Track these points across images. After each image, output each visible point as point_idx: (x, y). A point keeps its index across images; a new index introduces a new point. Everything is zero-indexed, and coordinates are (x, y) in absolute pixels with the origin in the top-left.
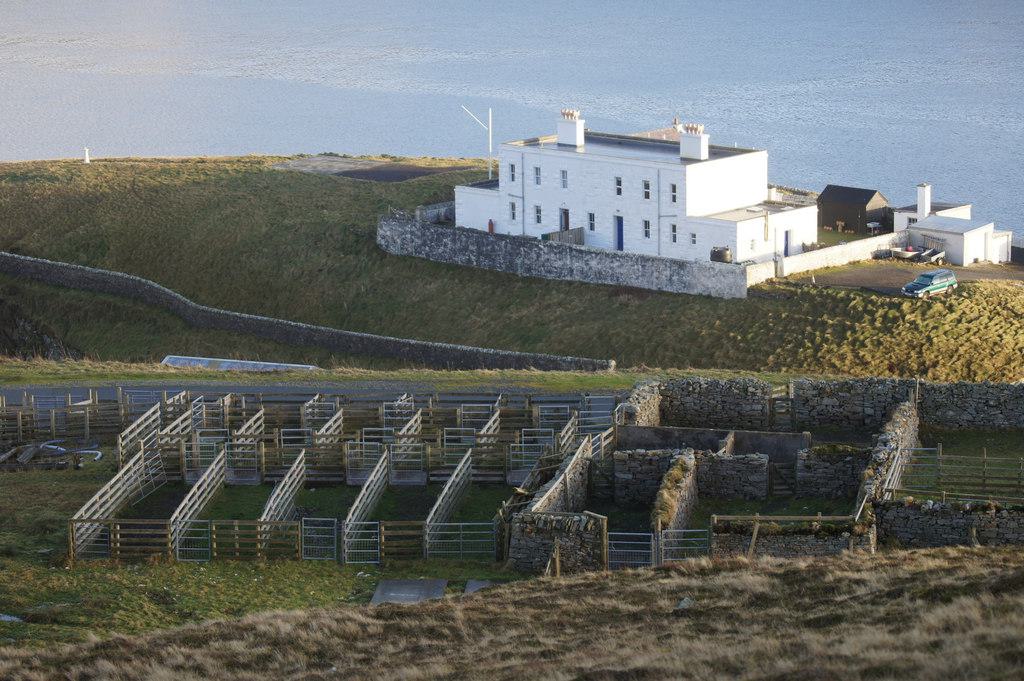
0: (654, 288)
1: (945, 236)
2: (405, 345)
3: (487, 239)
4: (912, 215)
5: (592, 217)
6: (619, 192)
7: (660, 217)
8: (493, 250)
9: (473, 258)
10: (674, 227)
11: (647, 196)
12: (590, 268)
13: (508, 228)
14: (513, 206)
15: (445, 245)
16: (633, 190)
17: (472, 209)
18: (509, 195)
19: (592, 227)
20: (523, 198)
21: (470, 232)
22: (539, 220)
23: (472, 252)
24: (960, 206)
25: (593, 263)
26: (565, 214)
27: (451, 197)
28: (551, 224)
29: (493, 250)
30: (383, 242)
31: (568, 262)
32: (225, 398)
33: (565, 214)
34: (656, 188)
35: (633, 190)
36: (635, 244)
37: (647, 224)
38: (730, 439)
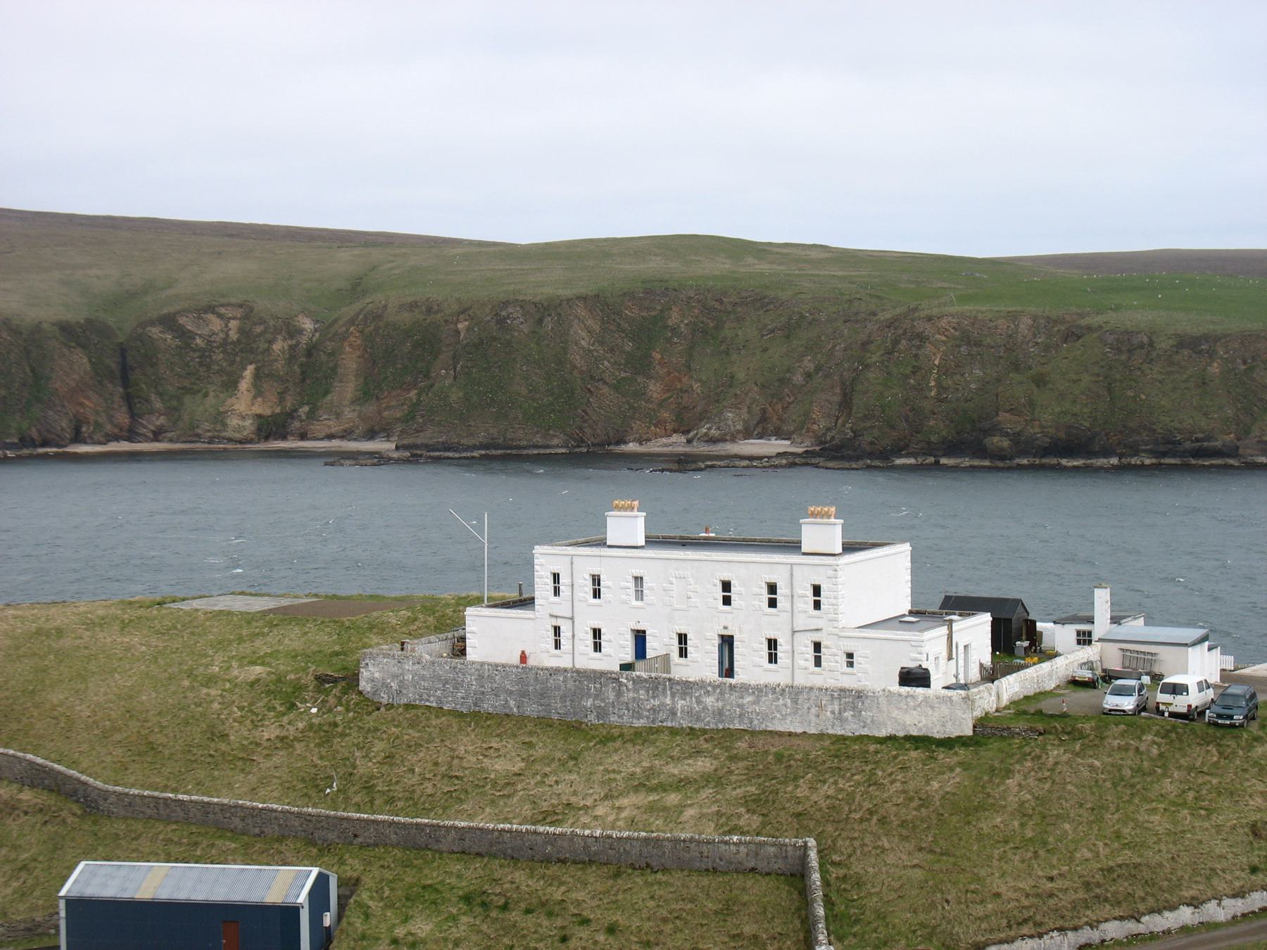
0: (813, 731)
1: (1152, 649)
2: (448, 829)
4: (1084, 627)
5: (682, 638)
6: (727, 601)
7: (794, 632)
10: (817, 647)
11: (772, 603)
12: (705, 708)
13: (545, 657)
14: (557, 630)
16: (749, 594)
18: (552, 616)
19: (683, 653)
20: (572, 618)
22: (597, 647)
25: (709, 701)
27: (460, 622)
28: (619, 650)
31: (668, 701)
34: (788, 592)
35: (749, 594)
37: (772, 644)
38: (249, 371)
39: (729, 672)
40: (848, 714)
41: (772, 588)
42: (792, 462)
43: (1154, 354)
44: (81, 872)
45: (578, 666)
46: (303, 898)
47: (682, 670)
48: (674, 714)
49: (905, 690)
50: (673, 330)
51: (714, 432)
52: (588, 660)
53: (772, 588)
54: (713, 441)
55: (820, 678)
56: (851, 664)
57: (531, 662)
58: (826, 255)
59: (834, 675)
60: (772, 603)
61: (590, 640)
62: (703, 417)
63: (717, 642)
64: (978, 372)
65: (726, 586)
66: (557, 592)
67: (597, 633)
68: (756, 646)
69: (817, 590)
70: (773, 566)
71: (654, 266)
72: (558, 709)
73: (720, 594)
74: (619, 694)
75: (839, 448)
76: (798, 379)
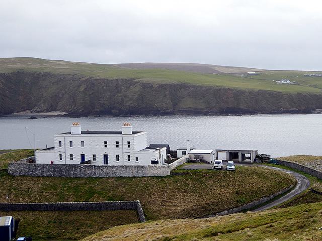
3: (53, 167)
5: (94, 156)
6: (106, 146)
8: (61, 169)
9: (52, 173)
10: (129, 156)
11: (117, 146)
13: (57, 162)
14: (61, 155)
15: (39, 170)
17: (41, 158)
19: (94, 159)
21: (43, 166)
23: (51, 171)
24: (206, 114)
25: (105, 170)
26: (83, 156)
28: (77, 161)
29: (61, 169)
30: (11, 172)
32: (161, 150)
33: (83, 156)
36: (112, 161)
37: (117, 156)
39: (107, 163)
40: (140, 172)
41: (117, 143)
42: (65, 116)
43: (153, 89)
44: (201, 149)
45: (67, 164)
46: (9, 224)
47: (94, 163)
48: (95, 174)
49: (154, 165)
50: (26, 83)
51: (38, 110)
52: (69, 162)
53: (117, 143)
54: (38, 112)
55: (129, 164)
56: (137, 160)
57: (54, 163)
58: (65, 63)
59: (133, 163)
60: (117, 146)
61: (69, 157)
62: (35, 106)
63: (103, 156)
64: (109, 93)
65: (106, 143)
66: (60, 146)
67: (71, 155)
68: (114, 157)
69: (129, 143)
70: (117, 137)
71: (19, 66)
72: (64, 174)
73: (104, 144)
74: (81, 170)
75: (72, 113)
76: (60, 96)
